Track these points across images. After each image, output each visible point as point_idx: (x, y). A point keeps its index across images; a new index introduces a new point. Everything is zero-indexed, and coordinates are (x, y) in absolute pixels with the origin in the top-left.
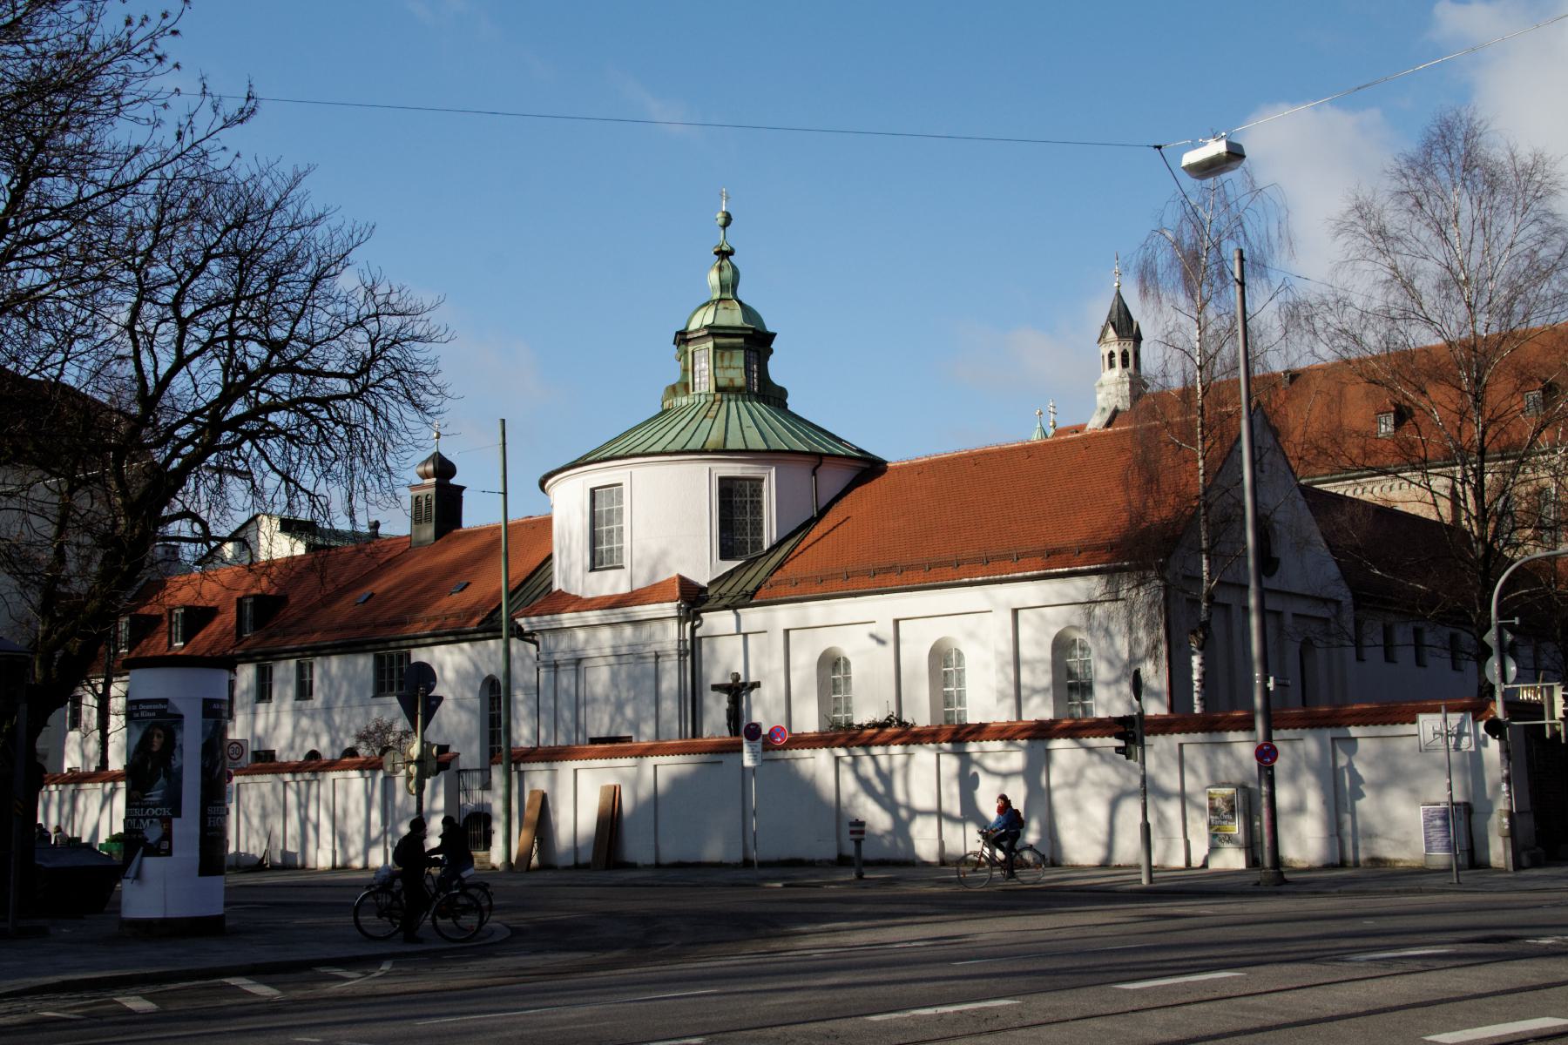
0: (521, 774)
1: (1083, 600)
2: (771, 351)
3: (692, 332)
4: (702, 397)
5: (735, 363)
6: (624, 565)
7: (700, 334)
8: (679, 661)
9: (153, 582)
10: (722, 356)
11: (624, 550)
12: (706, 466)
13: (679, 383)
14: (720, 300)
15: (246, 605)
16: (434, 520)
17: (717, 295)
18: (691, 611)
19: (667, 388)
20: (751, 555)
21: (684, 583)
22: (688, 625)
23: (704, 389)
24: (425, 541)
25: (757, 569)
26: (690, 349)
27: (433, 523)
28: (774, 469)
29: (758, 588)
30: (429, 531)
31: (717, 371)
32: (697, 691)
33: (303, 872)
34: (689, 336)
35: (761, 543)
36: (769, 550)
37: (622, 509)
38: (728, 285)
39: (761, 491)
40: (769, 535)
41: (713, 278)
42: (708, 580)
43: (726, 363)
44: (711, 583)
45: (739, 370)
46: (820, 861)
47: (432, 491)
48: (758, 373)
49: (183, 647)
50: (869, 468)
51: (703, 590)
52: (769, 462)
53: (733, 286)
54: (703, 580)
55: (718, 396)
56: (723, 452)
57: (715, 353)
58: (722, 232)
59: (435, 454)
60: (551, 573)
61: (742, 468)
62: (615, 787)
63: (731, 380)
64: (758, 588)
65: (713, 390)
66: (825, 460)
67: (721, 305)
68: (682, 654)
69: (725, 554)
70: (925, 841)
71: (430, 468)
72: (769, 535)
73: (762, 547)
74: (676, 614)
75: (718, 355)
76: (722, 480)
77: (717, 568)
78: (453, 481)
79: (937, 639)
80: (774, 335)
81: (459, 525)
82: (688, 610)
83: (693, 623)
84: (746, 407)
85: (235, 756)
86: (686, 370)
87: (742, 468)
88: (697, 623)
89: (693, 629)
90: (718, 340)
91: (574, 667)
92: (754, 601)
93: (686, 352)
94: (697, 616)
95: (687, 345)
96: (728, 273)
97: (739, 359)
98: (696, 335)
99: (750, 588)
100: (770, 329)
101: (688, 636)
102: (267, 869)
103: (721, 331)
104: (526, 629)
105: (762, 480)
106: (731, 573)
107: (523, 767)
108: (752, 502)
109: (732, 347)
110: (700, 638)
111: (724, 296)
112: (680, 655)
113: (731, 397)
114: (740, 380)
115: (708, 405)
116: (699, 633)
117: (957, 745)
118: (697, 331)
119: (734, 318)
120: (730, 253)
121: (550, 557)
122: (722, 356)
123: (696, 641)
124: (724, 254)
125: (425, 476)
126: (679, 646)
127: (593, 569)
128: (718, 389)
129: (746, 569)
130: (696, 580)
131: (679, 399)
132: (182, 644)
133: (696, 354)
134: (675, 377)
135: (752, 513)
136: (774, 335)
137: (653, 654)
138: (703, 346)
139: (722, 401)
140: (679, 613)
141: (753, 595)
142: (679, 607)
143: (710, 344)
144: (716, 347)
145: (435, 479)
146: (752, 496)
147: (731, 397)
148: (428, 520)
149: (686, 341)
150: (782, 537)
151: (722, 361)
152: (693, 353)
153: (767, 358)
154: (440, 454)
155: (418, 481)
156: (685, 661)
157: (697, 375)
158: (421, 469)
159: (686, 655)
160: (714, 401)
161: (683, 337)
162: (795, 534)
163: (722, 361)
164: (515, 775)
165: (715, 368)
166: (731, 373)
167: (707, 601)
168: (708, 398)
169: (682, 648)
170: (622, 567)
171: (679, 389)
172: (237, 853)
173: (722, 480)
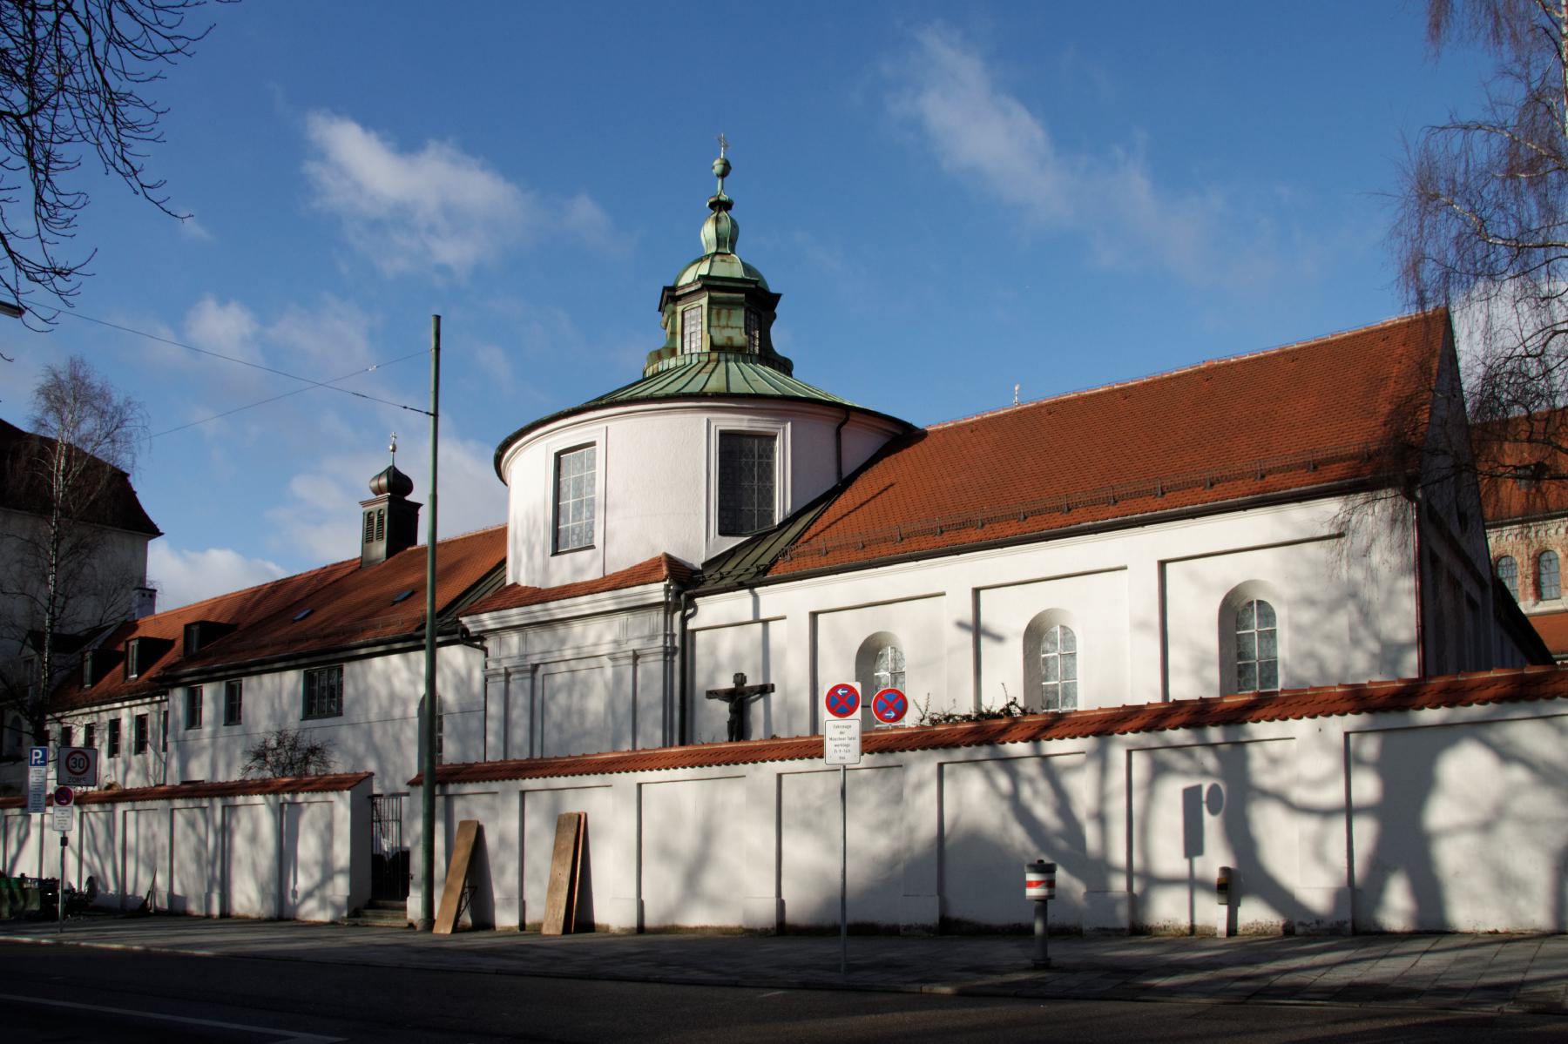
0: (449, 799)
1: (1325, 532)
2: (775, 317)
3: (683, 287)
4: (695, 357)
5: (732, 323)
6: (595, 544)
7: (693, 289)
8: (665, 661)
9: (130, 622)
10: (718, 314)
11: (597, 502)
12: (704, 417)
13: (665, 348)
14: (716, 253)
15: (193, 631)
16: (385, 536)
17: (713, 250)
18: (682, 597)
19: (651, 354)
20: (757, 531)
21: (672, 562)
22: (678, 615)
23: (695, 347)
24: (377, 560)
25: (767, 546)
26: (679, 309)
27: (385, 540)
28: (789, 424)
29: (774, 562)
30: (380, 548)
31: (712, 330)
32: (688, 706)
33: (207, 921)
34: (679, 293)
35: (771, 515)
36: (782, 525)
37: (593, 474)
38: (726, 238)
39: (772, 450)
40: (782, 506)
41: (708, 232)
42: (703, 560)
43: (723, 322)
44: (707, 564)
45: (738, 330)
46: (908, 928)
47: (384, 505)
48: (760, 339)
49: (137, 679)
50: (901, 436)
51: (696, 572)
52: (782, 416)
54: (697, 558)
55: (714, 356)
56: (726, 398)
57: (710, 310)
58: (720, 181)
59: (390, 468)
60: (505, 576)
61: (750, 420)
62: (580, 817)
63: (730, 338)
64: (774, 562)
65: (706, 348)
66: (854, 417)
67: (717, 258)
68: (668, 653)
69: (724, 531)
70: (1169, 909)
71: (384, 481)
72: (782, 506)
73: (772, 522)
74: (663, 599)
75: (714, 312)
76: (725, 436)
77: (715, 545)
78: (410, 498)
79: (1049, 607)
80: (777, 297)
81: (415, 543)
82: (678, 594)
83: (684, 612)
84: (749, 367)
85: (77, 770)
86: (673, 333)
87: (750, 420)
88: (689, 611)
89: (684, 620)
90: (715, 294)
91: (529, 675)
92: (769, 576)
93: (674, 313)
94: (690, 602)
95: (676, 305)
96: (725, 225)
97: (739, 318)
98: (687, 290)
99: (765, 560)
100: (773, 289)
101: (677, 629)
102: (151, 915)
103: (718, 283)
104: (472, 629)
105: (774, 437)
106: (732, 553)
107: (451, 789)
108: (760, 464)
109: (731, 304)
110: (694, 631)
111: (720, 251)
112: (666, 654)
113: (729, 356)
114: (739, 338)
115: (701, 365)
116: (691, 625)
117: (1233, 729)
118: (689, 285)
119: (732, 268)
120: (727, 206)
121: (504, 561)
122: (718, 314)
123: (688, 637)
124: (721, 206)
125: (378, 491)
126: (665, 642)
127: (555, 553)
128: (713, 347)
129: (752, 547)
130: (690, 561)
131: (666, 361)
132: (135, 676)
133: (687, 315)
134: (660, 341)
136: (777, 297)
137: (631, 653)
138: (696, 304)
139: (718, 361)
140: (667, 596)
141: (767, 570)
142: (667, 589)
143: (704, 301)
144: (711, 302)
145: (389, 494)
146: (760, 456)
147: (729, 356)
148: (380, 537)
149: (675, 299)
150: (798, 508)
151: (719, 319)
152: (683, 313)
153: (770, 323)
154: (395, 468)
155: (373, 496)
156: (672, 661)
157: (687, 340)
158: (375, 484)
159: (673, 654)
160: (709, 361)
161: (671, 293)
162: (812, 507)
163: (719, 319)
164: (440, 801)
165: (709, 326)
166: (728, 333)
167: (702, 583)
168: (701, 359)
169: (668, 644)
170: (592, 547)
171: (664, 353)
172: (134, 895)
173: (725, 436)
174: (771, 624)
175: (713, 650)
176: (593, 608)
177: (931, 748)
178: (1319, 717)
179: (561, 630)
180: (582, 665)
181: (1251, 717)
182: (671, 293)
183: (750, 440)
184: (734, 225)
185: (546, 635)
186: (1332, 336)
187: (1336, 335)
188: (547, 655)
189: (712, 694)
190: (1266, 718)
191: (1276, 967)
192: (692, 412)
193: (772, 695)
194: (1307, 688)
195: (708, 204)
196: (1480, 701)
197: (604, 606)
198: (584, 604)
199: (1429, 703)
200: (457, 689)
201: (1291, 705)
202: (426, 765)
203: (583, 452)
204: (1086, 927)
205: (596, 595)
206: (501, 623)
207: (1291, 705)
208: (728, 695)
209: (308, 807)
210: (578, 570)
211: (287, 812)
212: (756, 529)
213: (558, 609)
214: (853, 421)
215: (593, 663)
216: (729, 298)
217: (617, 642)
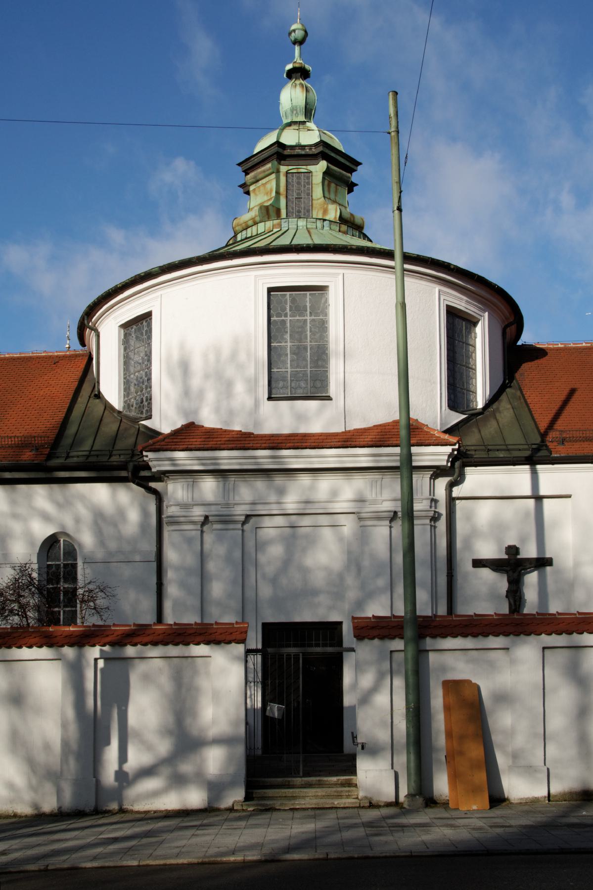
91: (199, 527)
161: (280, 150)
174: (545, 501)
175: (469, 517)
176: (240, 464)
177: (214, 643)
178: (553, 635)
179: (279, 480)
180: (306, 521)
181: (89, 642)
182: (280, 150)
183: (460, 321)
185: (260, 484)
186: (32, 353)
187: (35, 353)
188: (309, 506)
189: (478, 563)
190: (27, 645)
191: (37, 852)
192: (417, 278)
193: (548, 568)
194: (214, 622)
195: (285, 76)
196: (132, 644)
197: (164, 465)
198: (330, 457)
199: (37, 644)
200: (99, 532)
201: (14, 638)
202: (409, 609)
203: (286, 295)
204: (380, 804)
205: (350, 449)
206: (203, 464)
207: (14, 638)
208: (495, 565)
209: (237, 658)
210: (301, 417)
211: (102, 670)
213: (292, 458)
214: (98, 326)
215: (324, 520)
216: (340, 173)
217: (361, 500)
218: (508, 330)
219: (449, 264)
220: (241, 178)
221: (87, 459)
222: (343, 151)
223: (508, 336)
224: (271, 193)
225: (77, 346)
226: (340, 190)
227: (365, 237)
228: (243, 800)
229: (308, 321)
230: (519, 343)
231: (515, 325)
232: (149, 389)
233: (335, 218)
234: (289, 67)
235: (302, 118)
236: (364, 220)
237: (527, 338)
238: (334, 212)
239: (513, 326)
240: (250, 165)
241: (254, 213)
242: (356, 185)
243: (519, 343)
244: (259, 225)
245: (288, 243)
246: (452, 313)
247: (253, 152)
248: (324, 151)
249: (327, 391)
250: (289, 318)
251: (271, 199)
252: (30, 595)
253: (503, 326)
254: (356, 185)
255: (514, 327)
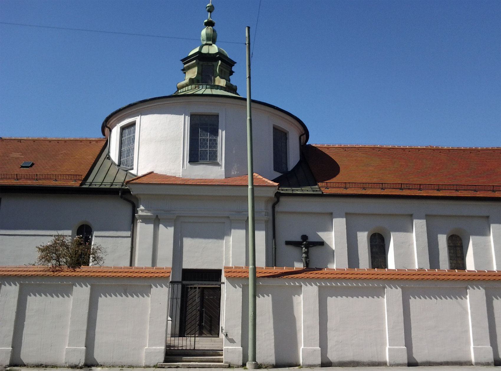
53: (213, 39)
108: (210, 126)
135: (210, 147)
184: (214, 31)
195: (204, 25)
212: (208, 161)
218: (302, 137)
219: (275, 106)
220: (183, 66)
221: (111, 186)
222: (229, 57)
223: (302, 141)
224: (195, 73)
225: (102, 137)
226: (198, 346)
227: (238, 94)
228: (163, 362)
229: (209, 128)
230: (307, 144)
231: (305, 135)
232: (132, 156)
233: (224, 85)
234: (206, 21)
235: (211, 42)
236: (237, 87)
237: (310, 142)
238: (223, 82)
239: (304, 136)
240: (186, 60)
241: (187, 81)
242: (236, 63)
243: (307, 144)
244: (189, 86)
245: (201, 93)
246: (276, 130)
247: (188, 55)
248: (220, 56)
249: (217, 160)
250: (208, 149)
251: (195, 75)
252: (77, 245)
253: (300, 135)
254: (236, 63)
255: (305, 136)
